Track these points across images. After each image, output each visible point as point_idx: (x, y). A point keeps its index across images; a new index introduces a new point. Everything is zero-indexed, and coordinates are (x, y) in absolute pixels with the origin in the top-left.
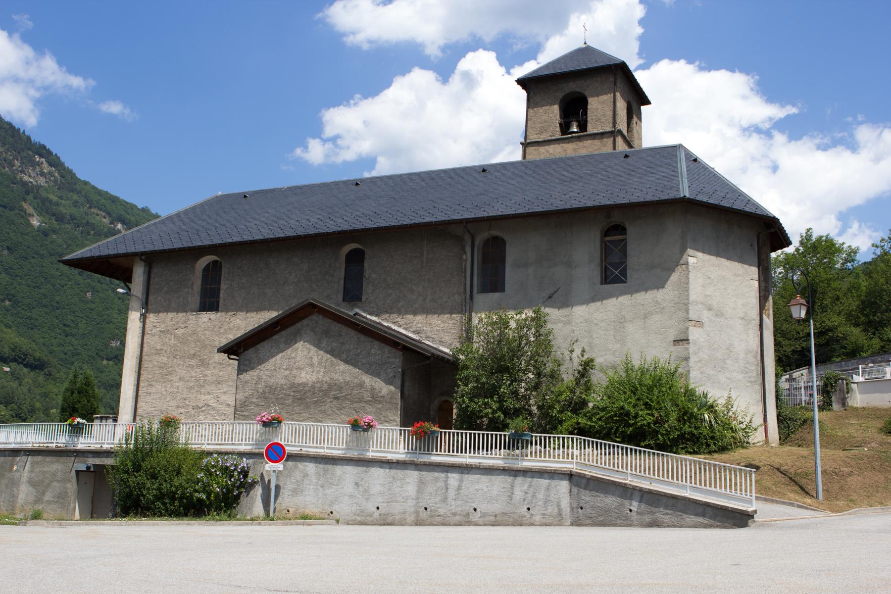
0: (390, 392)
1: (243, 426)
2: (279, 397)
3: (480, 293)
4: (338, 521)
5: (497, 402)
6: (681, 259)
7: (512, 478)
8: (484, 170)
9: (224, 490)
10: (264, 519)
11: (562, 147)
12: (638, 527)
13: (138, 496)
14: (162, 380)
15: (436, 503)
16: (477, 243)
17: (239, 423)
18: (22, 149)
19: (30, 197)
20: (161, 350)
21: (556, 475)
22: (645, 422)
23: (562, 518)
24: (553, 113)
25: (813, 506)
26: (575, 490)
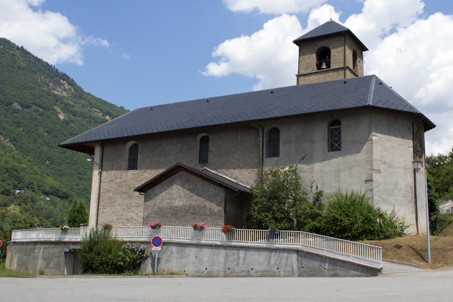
0: (219, 210)
1: (148, 229)
2: (165, 213)
3: (267, 157)
4: (187, 275)
5: (272, 214)
6: (368, 138)
7: (270, 253)
8: (272, 92)
9: (132, 260)
10: (152, 275)
12: (328, 277)
13: (92, 263)
14: (110, 206)
15: (234, 266)
16: (265, 131)
17: (146, 227)
18: (53, 76)
19: (58, 103)
20: (109, 190)
21: (291, 252)
22: (346, 224)
23: (294, 273)
24: (313, 58)
25: (422, 266)
26: (300, 259)
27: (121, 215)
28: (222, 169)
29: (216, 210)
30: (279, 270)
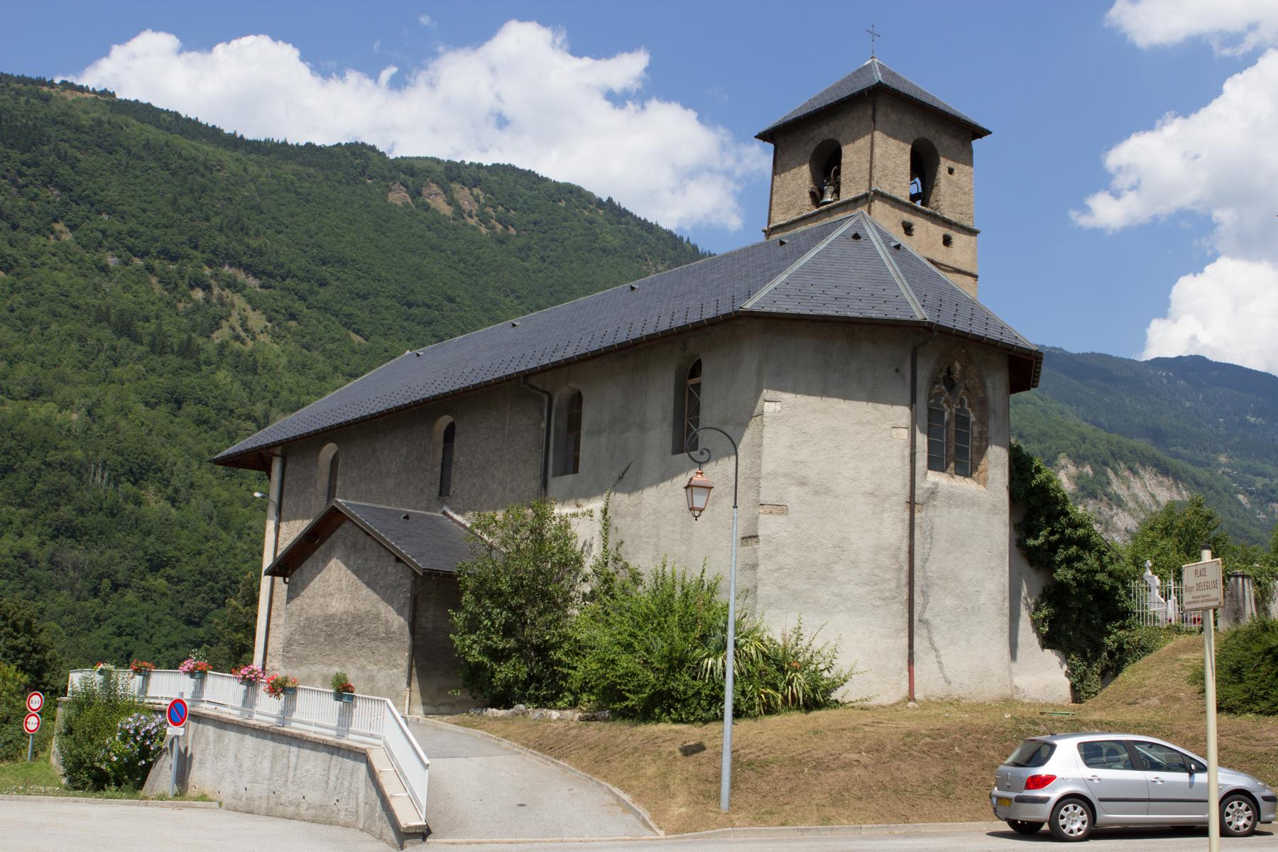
4: (220, 804)
6: (755, 407)
7: (330, 756)
16: (555, 403)
24: (801, 177)
29: (395, 626)
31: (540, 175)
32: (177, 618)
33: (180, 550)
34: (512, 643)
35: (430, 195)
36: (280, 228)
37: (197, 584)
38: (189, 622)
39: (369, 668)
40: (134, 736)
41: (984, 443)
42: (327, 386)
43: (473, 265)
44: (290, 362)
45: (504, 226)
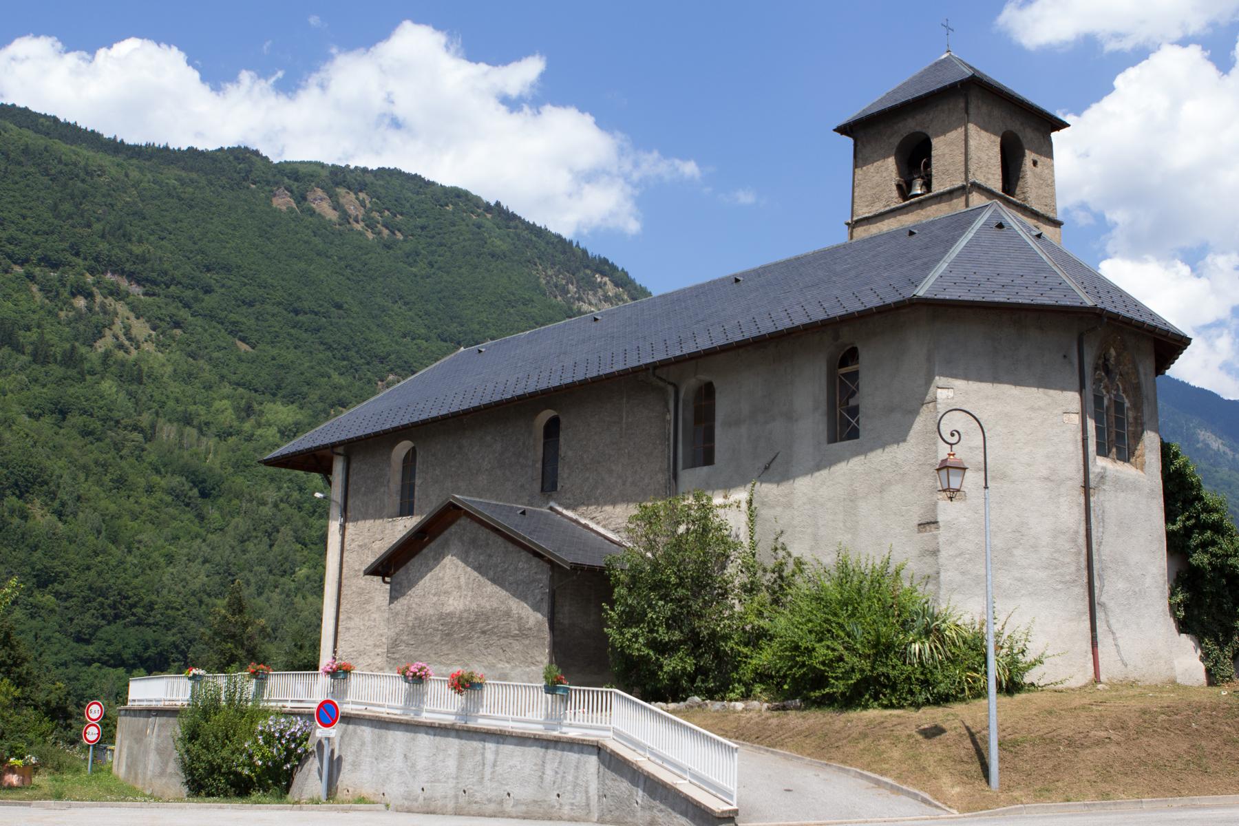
2: (428, 632)
4: (387, 806)
6: (926, 394)
7: (543, 750)
11: (899, 221)
16: (682, 395)
24: (887, 170)
27: (382, 636)
28: (588, 505)
29: (532, 622)
30: (561, 800)
31: (426, 179)
32: (65, 633)
33: (68, 566)
34: (677, 635)
35: (315, 199)
36: (164, 234)
37: (87, 600)
38: (79, 639)
39: (499, 666)
40: (280, 739)
41: (1140, 429)
42: (215, 396)
43: (360, 271)
44: (175, 370)
45: (391, 231)
